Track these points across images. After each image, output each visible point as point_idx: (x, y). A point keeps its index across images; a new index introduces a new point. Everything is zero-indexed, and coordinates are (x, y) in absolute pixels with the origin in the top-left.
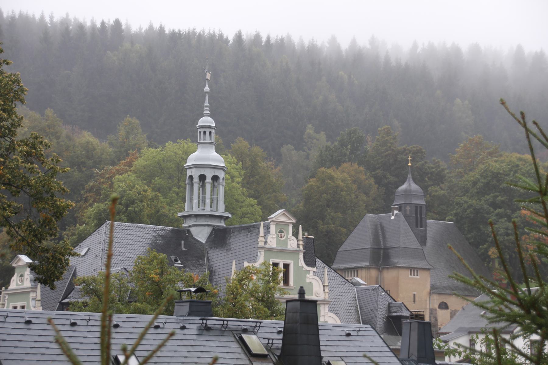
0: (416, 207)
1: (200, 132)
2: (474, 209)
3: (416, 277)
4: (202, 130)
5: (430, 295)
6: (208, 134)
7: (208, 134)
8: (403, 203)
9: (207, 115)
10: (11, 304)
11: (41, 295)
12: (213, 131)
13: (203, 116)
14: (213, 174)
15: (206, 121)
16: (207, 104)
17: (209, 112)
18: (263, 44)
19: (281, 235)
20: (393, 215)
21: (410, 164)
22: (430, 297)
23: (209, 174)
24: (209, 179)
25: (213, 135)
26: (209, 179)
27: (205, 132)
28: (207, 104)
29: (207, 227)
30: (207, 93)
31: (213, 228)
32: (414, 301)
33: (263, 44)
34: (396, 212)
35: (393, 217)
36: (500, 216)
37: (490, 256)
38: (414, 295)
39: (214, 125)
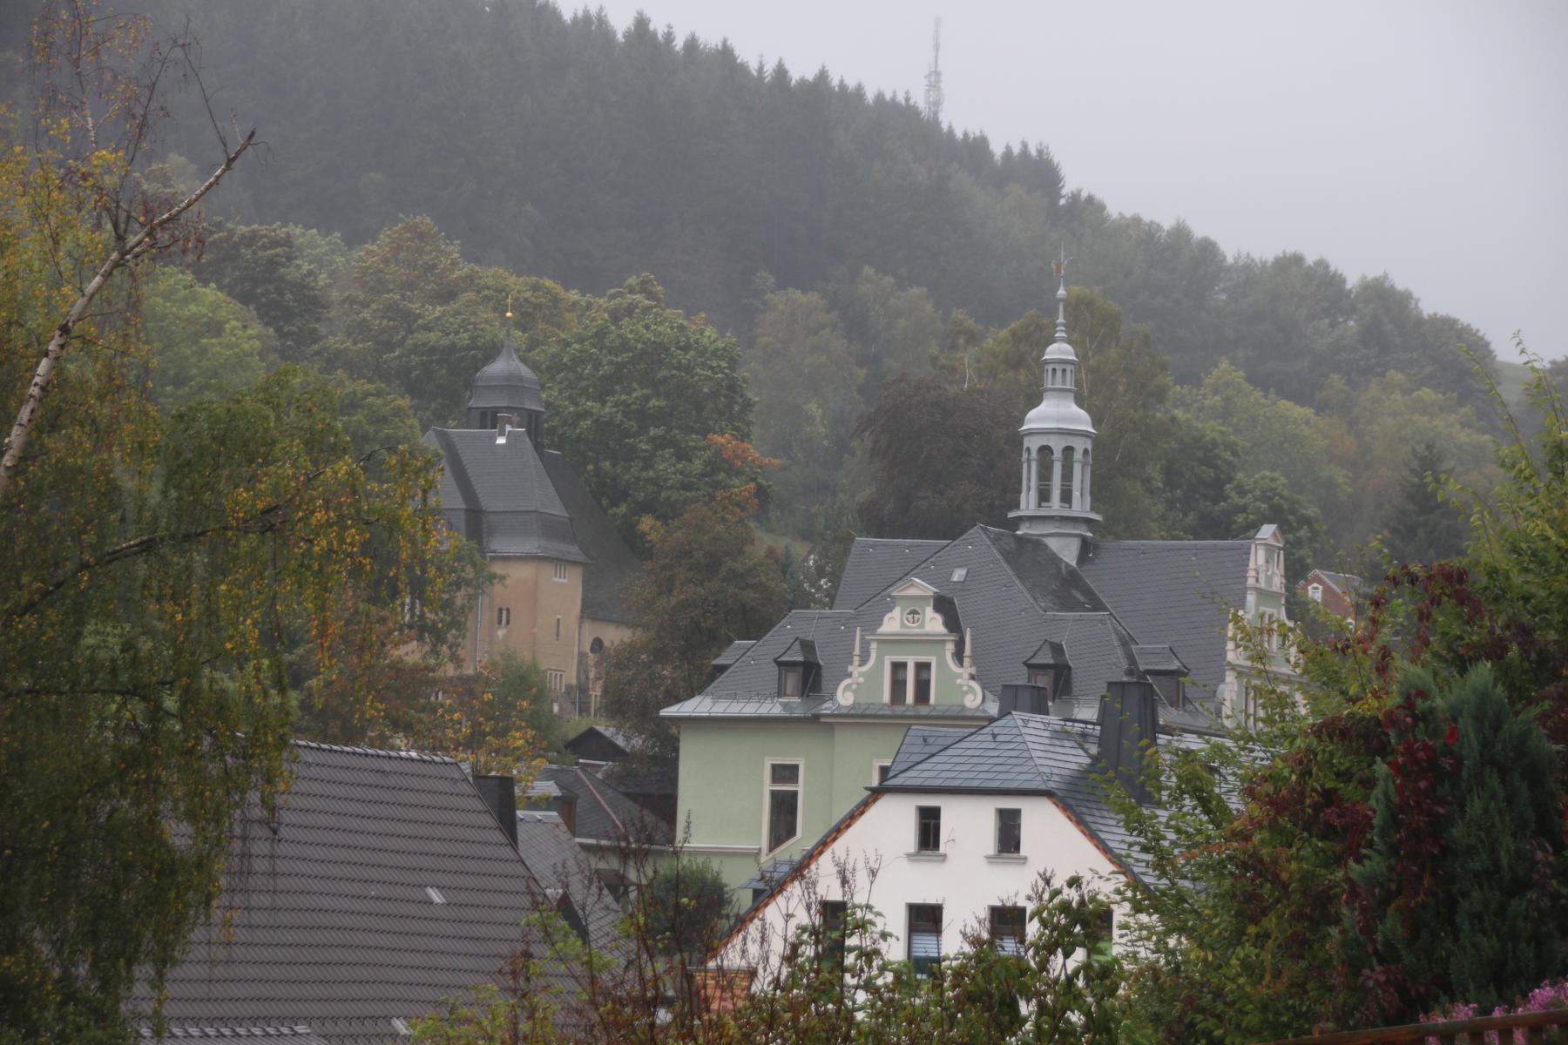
0: (530, 416)
1: (1054, 370)
2: (596, 421)
3: (562, 580)
4: (1050, 367)
5: (582, 622)
6: (1059, 373)
7: (1059, 373)
8: (506, 405)
9: (1062, 340)
10: (886, 657)
11: (972, 648)
12: (1069, 368)
13: (1053, 341)
14: (1064, 445)
15: (1059, 350)
16: (1061, 320)
17: (1064, 335)
18: (1063, 202)
20: (502, 434)
21: (509, 314)
22: (580, 627)
23: (1057, 445)
24: (1058, 454)
25: (1068, 372)
26: (1058, 454)
27: (1064, 371)
28: (1061, 320)
29: (1076, 539)
30: (1062, 300)
31: (879, 523)
32: (558, 635)
33: (1063, 202)
34: (508, 428)
35: (501, 441)
36: (660, 443)
37: (645, 534)
38: (558, 620)
39: (1073, 357)
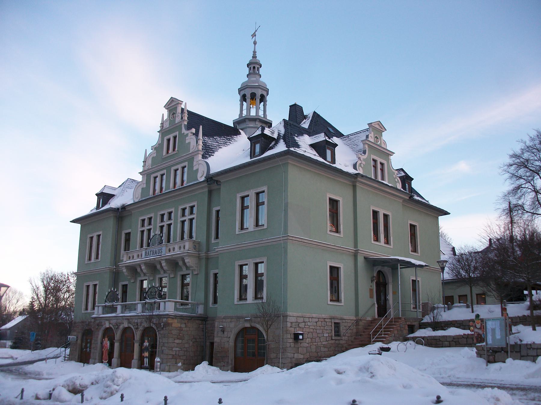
19: (173, 116)
